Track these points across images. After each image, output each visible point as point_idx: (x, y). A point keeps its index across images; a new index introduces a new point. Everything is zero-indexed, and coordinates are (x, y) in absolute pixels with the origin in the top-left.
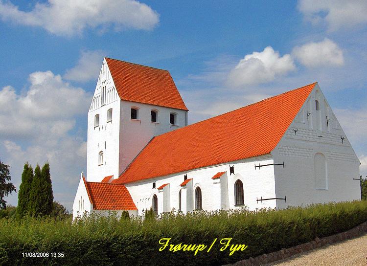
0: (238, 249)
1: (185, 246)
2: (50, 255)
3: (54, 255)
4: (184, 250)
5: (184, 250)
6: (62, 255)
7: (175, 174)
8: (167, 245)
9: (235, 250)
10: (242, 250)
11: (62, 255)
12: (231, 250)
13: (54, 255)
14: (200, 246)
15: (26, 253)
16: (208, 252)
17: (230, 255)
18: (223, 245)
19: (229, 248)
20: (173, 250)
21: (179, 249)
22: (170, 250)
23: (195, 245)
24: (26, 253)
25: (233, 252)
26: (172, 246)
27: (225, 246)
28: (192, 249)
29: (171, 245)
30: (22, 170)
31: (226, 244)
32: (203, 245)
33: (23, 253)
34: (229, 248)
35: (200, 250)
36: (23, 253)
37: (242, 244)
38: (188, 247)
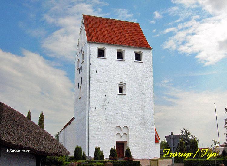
0: (212, 156)
1: (180, 154)
2: (22, 151)
3: (24, 151)
4: (179, 156)
5: (179, 156)
6: (28, 151)
7: (121, 142)
8: (168, 153)
9: (210, 156)
10: (215, 156)
11: (28, 151)
12: (208, 156)
13: (24, 151)
14: (189, 153)
15: (9, 150)
16: (194, 157)
17: (208, 159)
18: (203, 153)
19: (207, 154)
20: (172, 156)
21: (176, 156)
22: (170, 156)
23: (185, 153)
24: (9, 150)
25: (209, 157)
26: (171, 154)
27: (204, 154)
28: (184, 156)
29: (171, 153)
30: (150, 43)
31: (205, 152)
32: (191, 153)
33: (7, 150)
34: (207, 154)
35: (189, 156)
36: (7, 150)
37: (178, 152)
38: (181, 154)
